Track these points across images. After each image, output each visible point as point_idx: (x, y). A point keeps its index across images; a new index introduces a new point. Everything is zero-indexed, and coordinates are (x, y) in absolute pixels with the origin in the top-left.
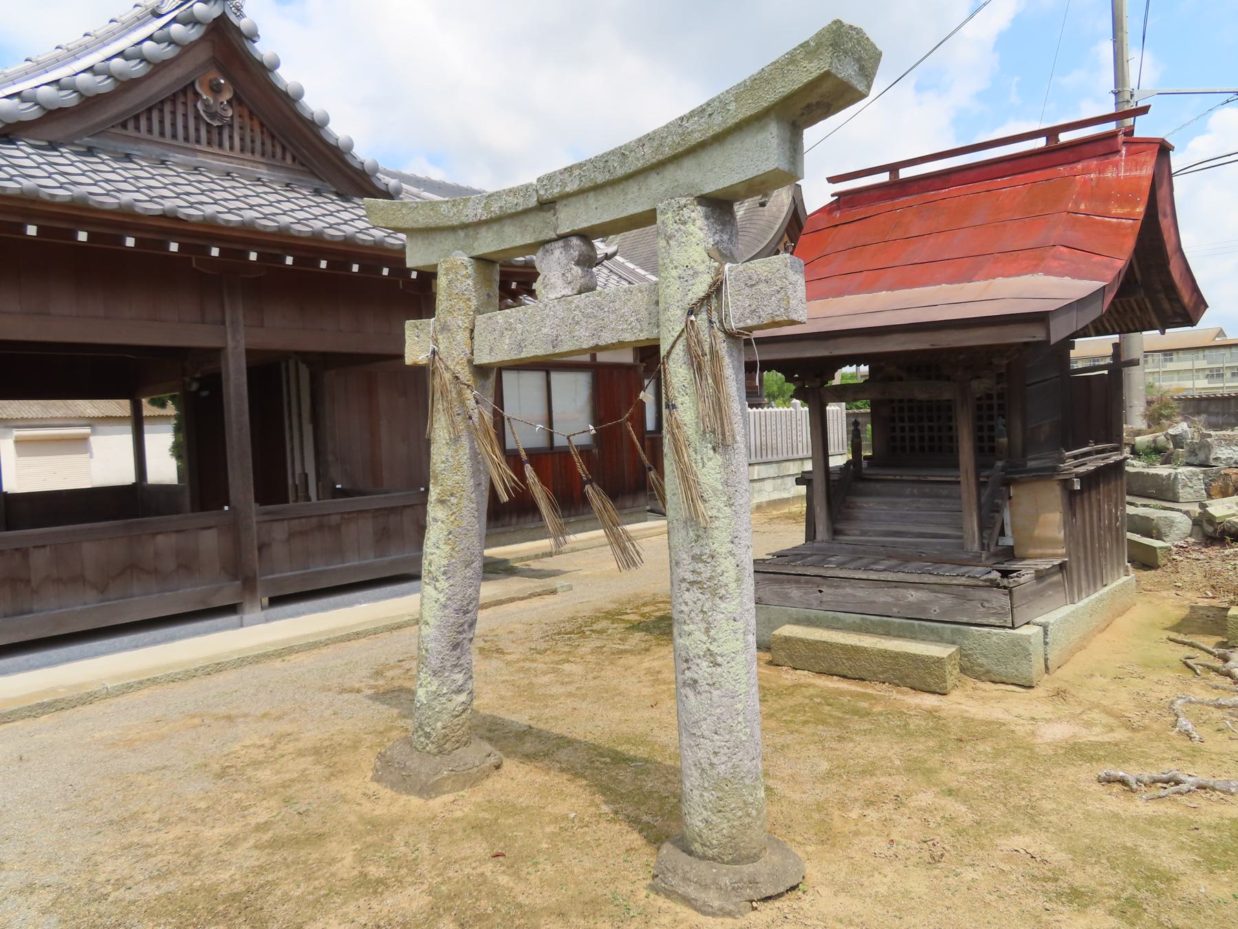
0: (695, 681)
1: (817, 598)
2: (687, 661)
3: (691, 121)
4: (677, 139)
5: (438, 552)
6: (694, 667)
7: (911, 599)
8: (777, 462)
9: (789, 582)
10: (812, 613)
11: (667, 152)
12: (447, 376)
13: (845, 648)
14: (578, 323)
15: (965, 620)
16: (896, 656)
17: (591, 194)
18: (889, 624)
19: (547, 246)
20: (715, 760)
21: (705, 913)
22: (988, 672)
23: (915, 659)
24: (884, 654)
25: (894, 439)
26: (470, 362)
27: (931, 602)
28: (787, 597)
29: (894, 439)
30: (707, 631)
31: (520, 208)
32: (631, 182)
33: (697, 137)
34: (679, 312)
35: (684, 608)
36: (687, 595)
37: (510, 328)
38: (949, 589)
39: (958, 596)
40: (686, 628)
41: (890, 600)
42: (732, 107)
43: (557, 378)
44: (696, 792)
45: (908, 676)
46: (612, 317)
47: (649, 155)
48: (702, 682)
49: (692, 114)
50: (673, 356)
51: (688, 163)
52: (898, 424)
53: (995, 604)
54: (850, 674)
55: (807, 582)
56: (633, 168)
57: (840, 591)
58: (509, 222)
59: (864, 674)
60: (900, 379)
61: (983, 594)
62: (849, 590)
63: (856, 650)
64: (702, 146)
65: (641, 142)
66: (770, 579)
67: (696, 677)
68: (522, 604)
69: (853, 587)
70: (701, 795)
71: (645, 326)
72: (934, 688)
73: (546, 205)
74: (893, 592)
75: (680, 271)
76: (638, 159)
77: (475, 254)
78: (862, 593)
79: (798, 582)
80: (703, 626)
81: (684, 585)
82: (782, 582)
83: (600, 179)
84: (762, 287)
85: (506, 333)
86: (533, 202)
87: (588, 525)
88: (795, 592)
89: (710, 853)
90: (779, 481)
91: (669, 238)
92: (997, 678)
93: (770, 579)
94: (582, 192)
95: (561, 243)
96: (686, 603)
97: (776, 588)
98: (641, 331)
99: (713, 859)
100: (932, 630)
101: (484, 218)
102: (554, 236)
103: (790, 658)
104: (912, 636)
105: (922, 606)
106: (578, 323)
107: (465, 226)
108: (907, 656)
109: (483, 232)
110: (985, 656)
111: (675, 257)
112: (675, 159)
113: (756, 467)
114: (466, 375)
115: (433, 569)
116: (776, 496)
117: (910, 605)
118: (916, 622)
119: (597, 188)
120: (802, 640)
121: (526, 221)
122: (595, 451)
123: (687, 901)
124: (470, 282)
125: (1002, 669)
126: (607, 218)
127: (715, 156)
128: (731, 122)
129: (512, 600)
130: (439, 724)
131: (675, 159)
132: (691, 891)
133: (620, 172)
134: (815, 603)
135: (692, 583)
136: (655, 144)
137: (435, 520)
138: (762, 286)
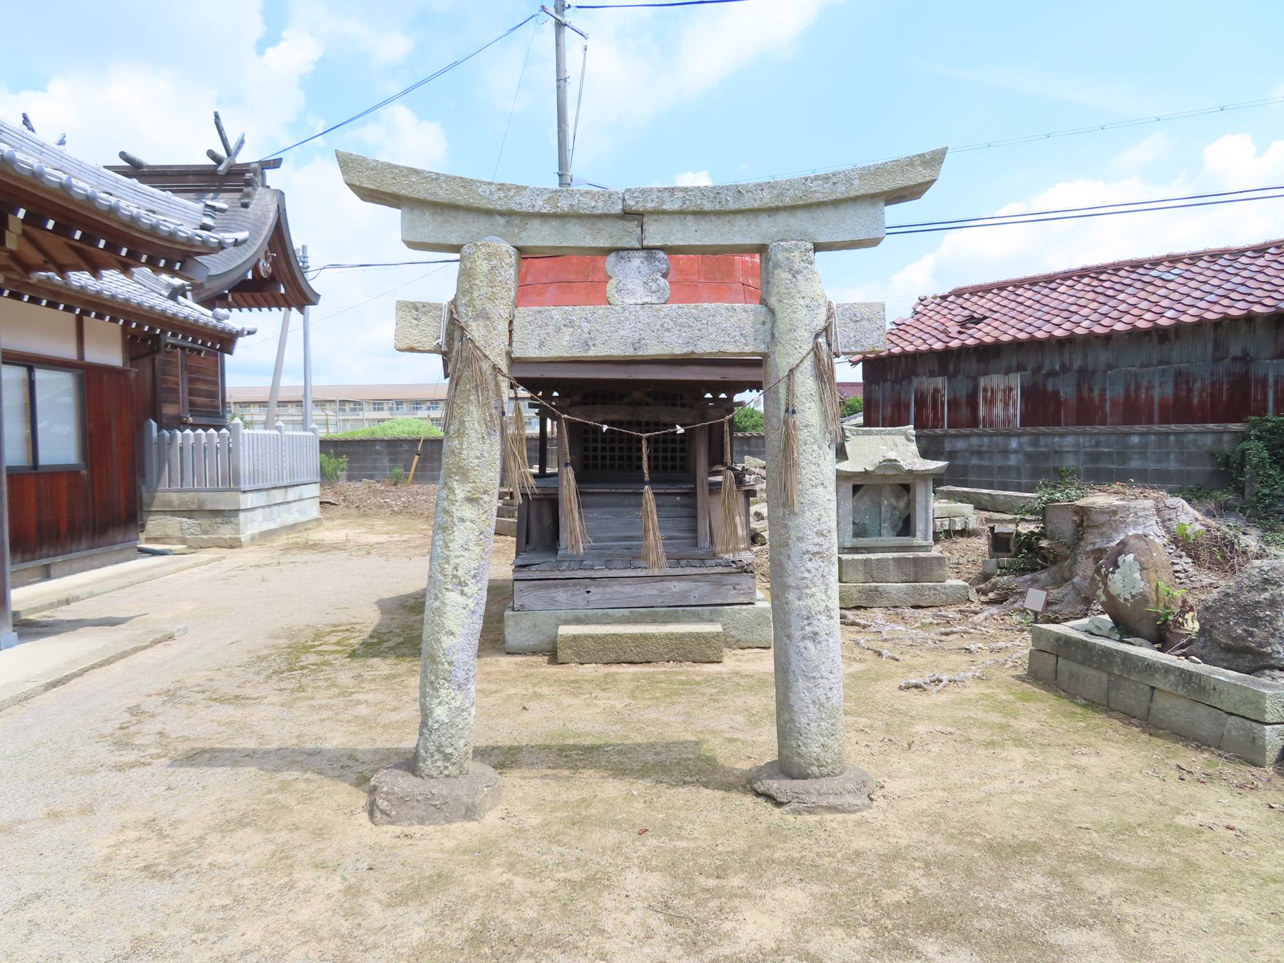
0: (816, 634)
1: (584, 599)
2: (808, 618)
3: (816, 183)
4: (799, 194)
5: (466, 554)
6: (815, 622)
7: (674, 590)
8: (267, 490)
9: (555, 586)
10: (581, 613)
11: (788, 201)
12: (486, 366)
13: (633, 637)
14: (668, 330)
15: (719, 602)
16: (682, 637)
17: (690, 218)
18: (656, 613)
19: (622, 253)
20: (830, 695)
21: (854, 812)
22: (738, 641)
23: (697, 637)
24: (669, 636)
25: (586, 458)
26: (509, 354)
27: (691, 590)
28: (553, 601)
29: (586, 458)
30: (826, 591)
31: (599, 212)
32: (739, 216)
33: (819, 197)
34: (806, 334)
35: (806, 575)
36: (809, 565)
37: (571, 324)
38: (707, 578)
39: (714, 583)
40: (808, 591)
41: (655, 592)
42: (856, 182)
43: (41, 375)
44: (813, 724)
45: (690, 652)
46: (712, 329)
47: (767, 199)
48: (822, 633)
49: (817, 178)
50: (800, 369)
51: (801, 214)
52: (591, 445)
53: (744, 586)
54: (637, 659)
55: (575, 585)
56: (748, 206)
57: (608, 589)
58: (575, 221)
59: (649, 657)
60: (647, 404)
61: (735, 579)
62: (617, 588)
63: (645, 637)
64: (820, 205)
65: (760, 187)
66: (534, 586)
67: (817, 629)
68: (148, 652)
69: (621, 584)
70: (819, 726)
71: (750, 340)
72: (712, 658)
73: (628, 215)
74: (658, 585)
75: (807, 301)
76: (755, 200)
77: (520, 244)
78: (629, 590)
79: (563, 586)
80: (823, 587)
81: (807, 557)
82: (549, 587)
83: (708, 206)
84: (865, 323)
85: (564, 329)
86: (618, 208)
87: (75, 565)
88: (561, 595)
89: (824, 770)
90: (267, 510)
91: (795, 274)
92: (745, 645)
93: (534, 586)
94: (682, 213)
95: (642, 253)
96: (809, 571)
97: (542, 593)
98: (746, 345)
99: (828, 775)
100: (694, 614)
101: (544, 211)
102: (638, 246)
103: (578, 654)
104: (677, 620)
105: (684, 595)
106: (668, 330)
107: (509, 214)
108: (691, 635)
109: (536, 223)
110: (736, 628)
111: (803, 288)
112: (792, 209)
113: (250, 495)
114: (503, 365)
115: (460, 573)
116: (266, 527)
117: (673, 594)
118: (679, 609)
119: (700, 214)
120: (592, 637)
121: (600, 225)
122: (84, 472)
123: (832, 809)
124: (512, 271)
125: (749, 637)
126: (707, 241)
127: (830, 215)
128: (853, 194)
129: (135, 650)
130: (462, 742)
131: (792, 209)
132: (832, 800)
133: (732, 206)
134: (583, 603)
135: (814, 554)
136: (776, 192)
137: (462, 520)
138: (865, 323)
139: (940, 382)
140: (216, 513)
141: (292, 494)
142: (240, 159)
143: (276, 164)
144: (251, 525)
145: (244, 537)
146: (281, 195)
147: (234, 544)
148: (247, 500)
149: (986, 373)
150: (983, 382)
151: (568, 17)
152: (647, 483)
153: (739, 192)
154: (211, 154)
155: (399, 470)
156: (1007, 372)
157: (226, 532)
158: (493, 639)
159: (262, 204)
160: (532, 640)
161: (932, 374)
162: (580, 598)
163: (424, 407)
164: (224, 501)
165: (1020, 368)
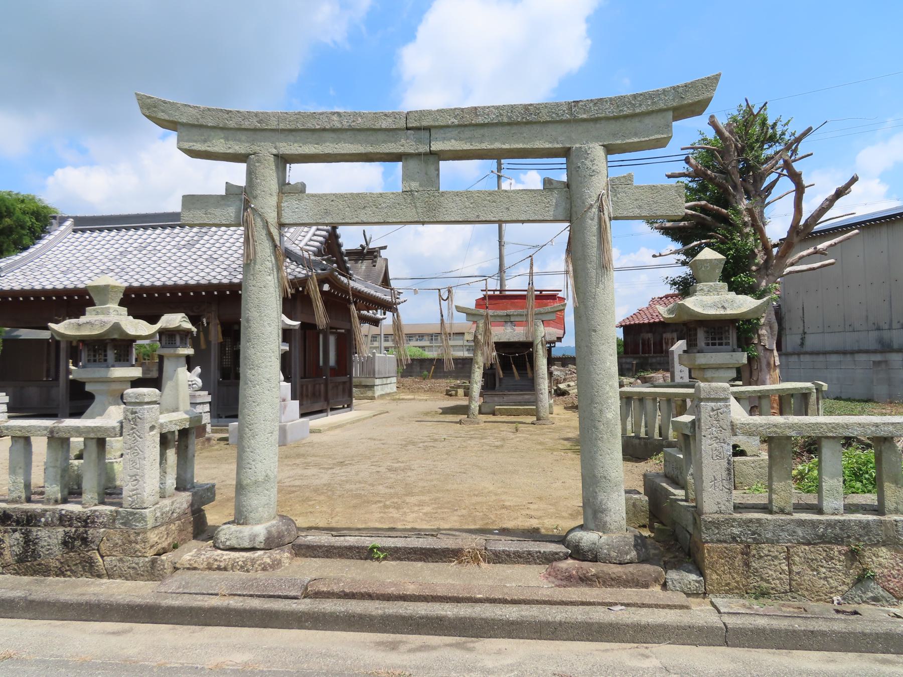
88: (496, 399)
139: (650, 335)
140: (366, 386)
141: (389, 380)
142: (371, 246)
143: (385, 248)
144: (378, 391)
145: (376, 395)
146: (386, 260)
147: (372, 398)
148: (378, 382)
149: (665, 332)
150: (664, 336)
151: (503, 173)
152: (6, 216)
153: (650, 96)
154: (361, 246)
155: (426, 373)
156: (672, 332)
157: (369, 394)
158: (480, 413)
159: (380, 263)
160: (488, 410)
161: (648, 332)
162: (501, 400)
163: (414, 339)
164: (368, 382)
165: (676, 331)
